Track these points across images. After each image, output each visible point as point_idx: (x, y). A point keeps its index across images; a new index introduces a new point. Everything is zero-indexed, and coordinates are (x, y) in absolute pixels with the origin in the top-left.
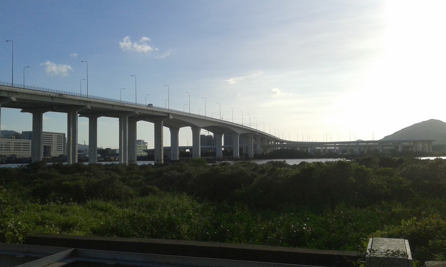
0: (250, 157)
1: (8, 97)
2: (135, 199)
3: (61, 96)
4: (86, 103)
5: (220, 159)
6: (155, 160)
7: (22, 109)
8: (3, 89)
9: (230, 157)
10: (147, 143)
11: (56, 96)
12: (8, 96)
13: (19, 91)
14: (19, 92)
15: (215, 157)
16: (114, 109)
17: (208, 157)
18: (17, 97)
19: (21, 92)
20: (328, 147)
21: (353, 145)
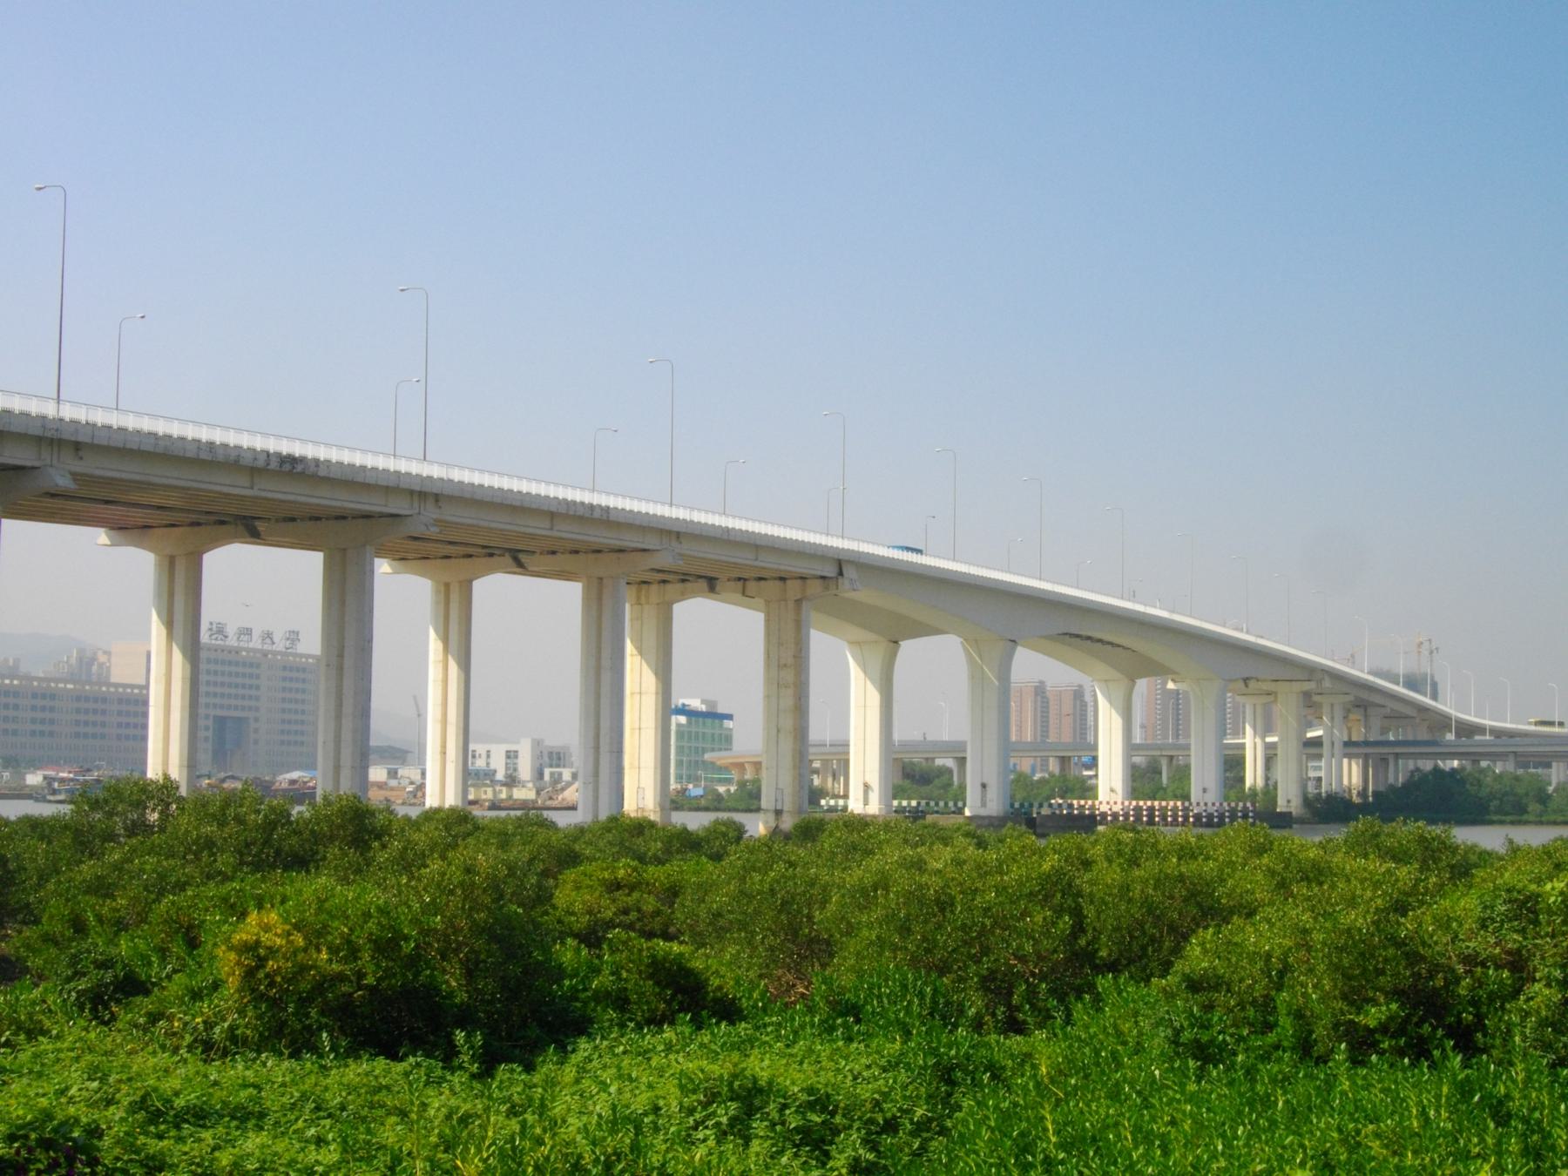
0: (1284, 810)
1: (33, 468)
2: (384, 1092)
3: (291, 467)
4: (416, 504)
5: (1210, 816)
6: (766, 811)
7: (383, 567)
8: (13, 429)
9: (1175, 809)
10: (730, 717)
11: (268, 464)
12: (36, 464)
13: (88, 440)
14: (87, 443)
15: (1090, 802)
16: (555, 533)
17: (1168, 804)
18: (78, 470)
19: (96, 442)
20: (199, 636)
21: (318, 505)
